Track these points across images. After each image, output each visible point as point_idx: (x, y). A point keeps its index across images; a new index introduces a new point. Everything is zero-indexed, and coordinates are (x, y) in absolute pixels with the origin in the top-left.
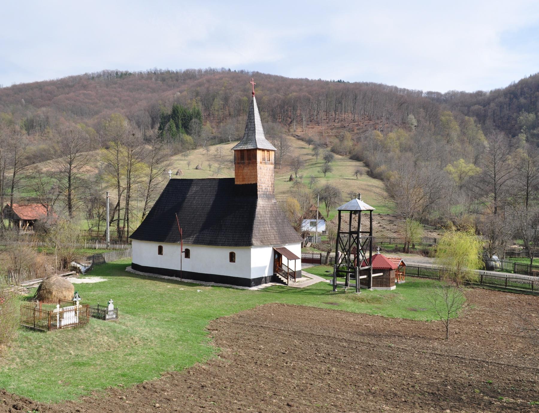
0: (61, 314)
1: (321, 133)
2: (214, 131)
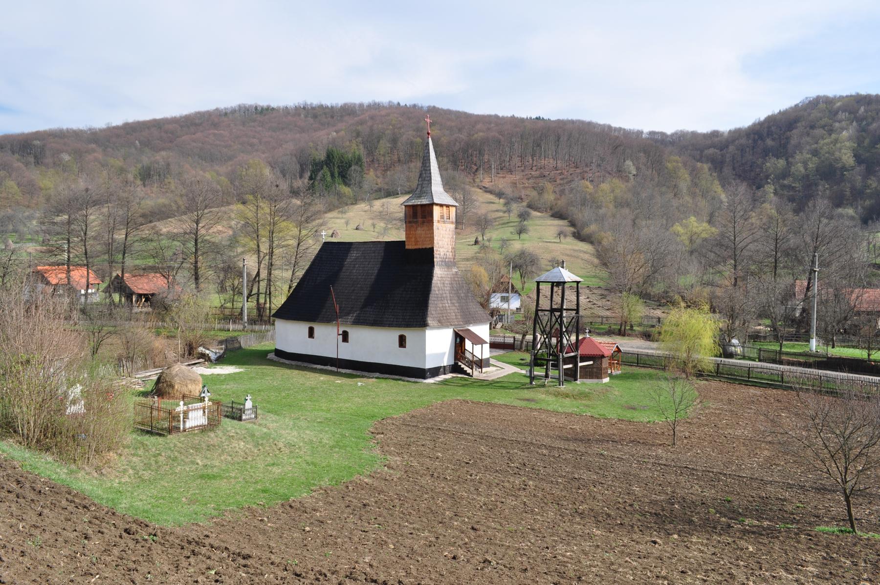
0: (186, 413)
1: (514, 184)
2: (379, 181)
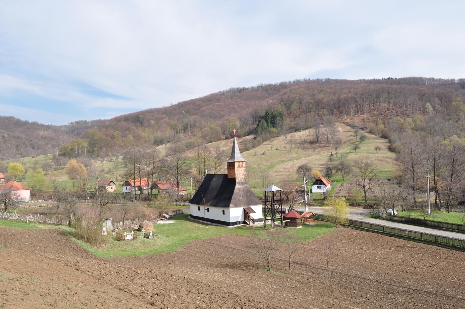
0: (126, 235)
1: (364, 120)
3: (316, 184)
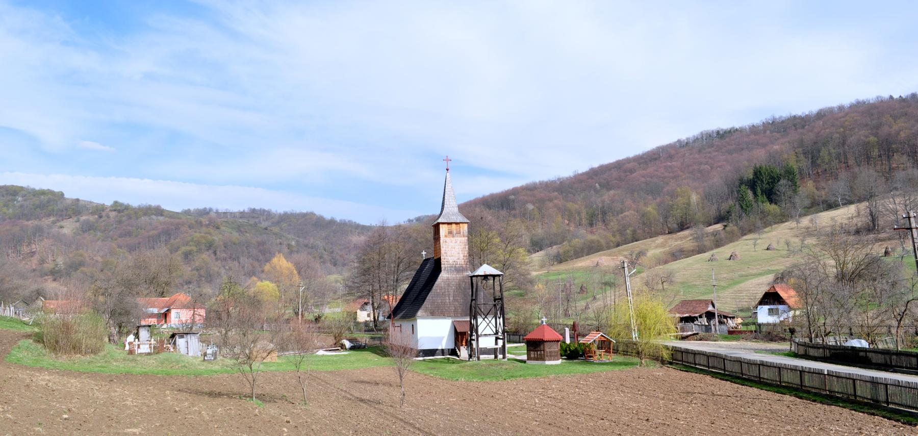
3: (766, 304)
